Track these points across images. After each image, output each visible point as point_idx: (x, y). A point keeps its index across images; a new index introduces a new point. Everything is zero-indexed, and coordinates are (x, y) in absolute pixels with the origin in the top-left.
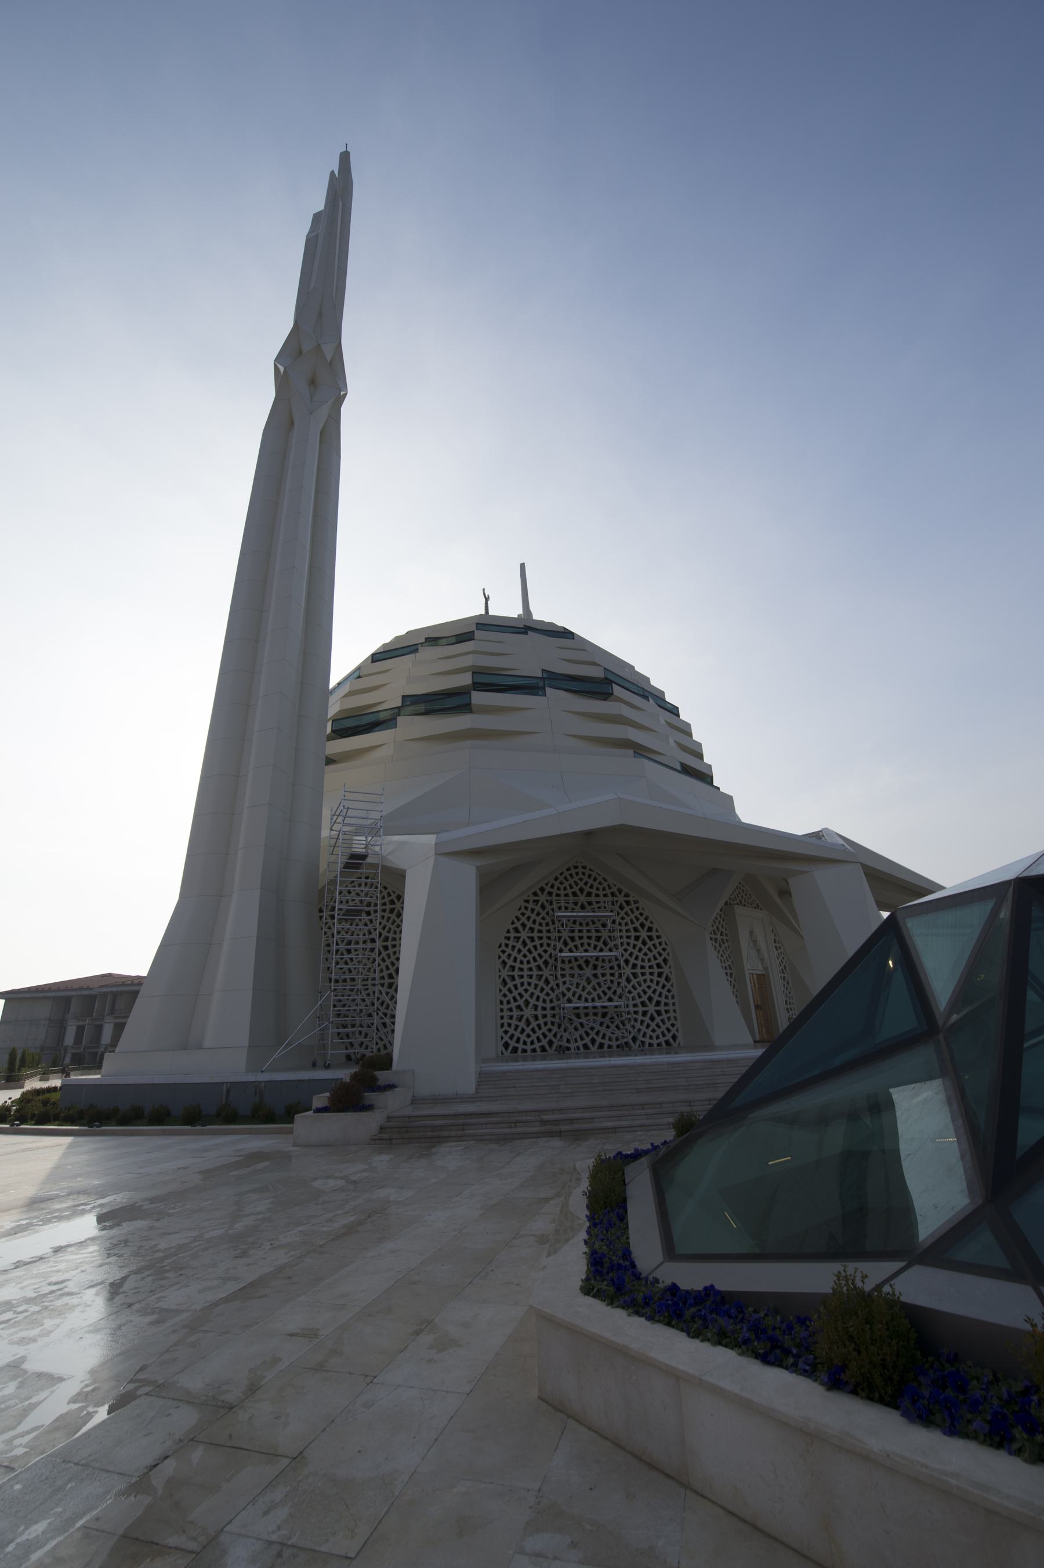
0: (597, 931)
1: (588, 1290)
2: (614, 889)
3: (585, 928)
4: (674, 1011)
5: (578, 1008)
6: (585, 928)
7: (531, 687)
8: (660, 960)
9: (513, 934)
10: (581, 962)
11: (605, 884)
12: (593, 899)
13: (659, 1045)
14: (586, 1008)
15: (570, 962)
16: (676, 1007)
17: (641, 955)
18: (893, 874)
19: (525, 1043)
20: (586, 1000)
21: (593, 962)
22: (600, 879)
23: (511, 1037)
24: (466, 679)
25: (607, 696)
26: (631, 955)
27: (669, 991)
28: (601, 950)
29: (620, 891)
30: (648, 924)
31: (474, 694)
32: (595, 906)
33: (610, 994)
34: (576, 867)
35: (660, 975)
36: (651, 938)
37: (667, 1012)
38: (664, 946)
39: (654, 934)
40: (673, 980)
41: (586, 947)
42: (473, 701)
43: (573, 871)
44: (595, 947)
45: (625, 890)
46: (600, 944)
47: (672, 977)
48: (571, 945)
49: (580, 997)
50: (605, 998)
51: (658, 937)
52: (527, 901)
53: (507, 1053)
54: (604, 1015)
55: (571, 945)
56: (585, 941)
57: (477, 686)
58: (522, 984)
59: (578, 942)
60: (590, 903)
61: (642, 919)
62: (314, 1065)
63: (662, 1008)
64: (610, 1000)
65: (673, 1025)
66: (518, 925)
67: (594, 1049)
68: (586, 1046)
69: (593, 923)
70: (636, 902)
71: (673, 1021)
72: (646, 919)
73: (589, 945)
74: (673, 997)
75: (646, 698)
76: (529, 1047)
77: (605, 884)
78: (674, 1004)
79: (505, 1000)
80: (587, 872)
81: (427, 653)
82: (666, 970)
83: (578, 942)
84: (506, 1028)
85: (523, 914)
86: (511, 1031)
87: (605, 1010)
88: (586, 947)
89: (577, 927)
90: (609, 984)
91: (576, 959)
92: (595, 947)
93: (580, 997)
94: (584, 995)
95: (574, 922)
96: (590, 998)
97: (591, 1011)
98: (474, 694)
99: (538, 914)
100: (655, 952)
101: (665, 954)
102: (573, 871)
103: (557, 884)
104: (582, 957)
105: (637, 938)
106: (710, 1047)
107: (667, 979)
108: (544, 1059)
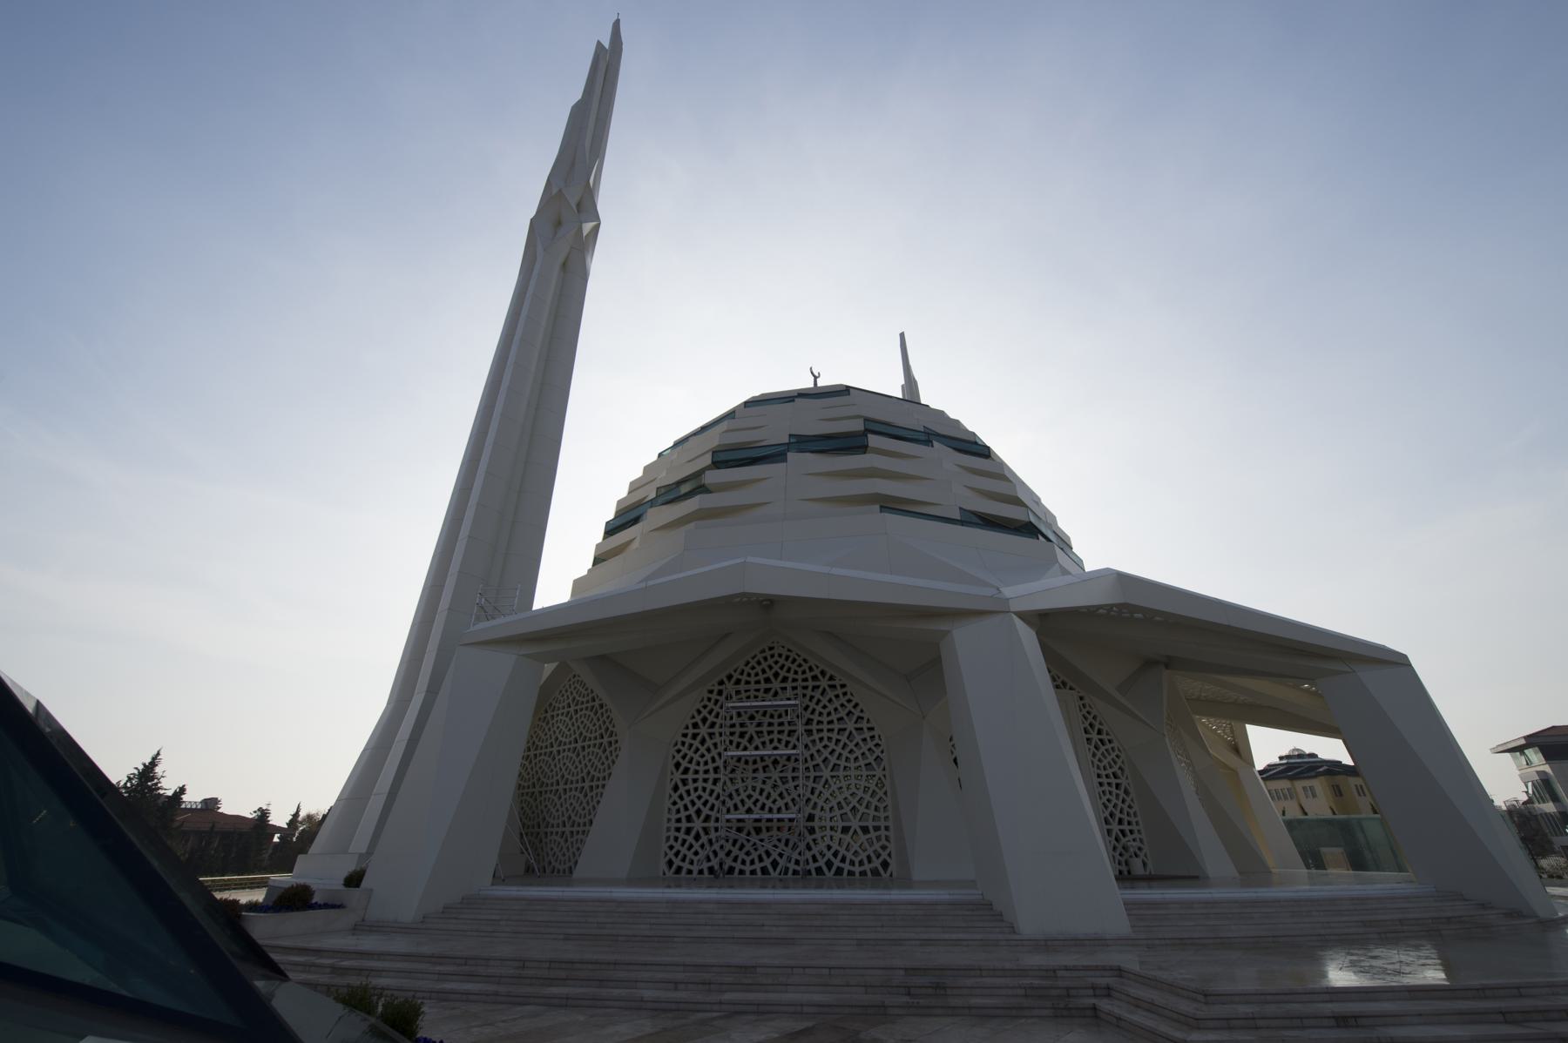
2: (817, 672)
3: (776, 721)
4: (887, 828)
6: (776, 721)
7: (775, 455)
8: (682, 790)
10: (769, 762)
11: (806, 667)
12: (742, 687)
13: (753, 872)
14: (769, 820)
15: (755, 762)
16: (1141, 827)
17: (845, 753)
18: (1233, 624)
19: (743, 862)
20: (771, 810)
22: (799, 660)
23: (677, 854)
24: (858, 426)
25: (864, 449)
27: (671, 847)
28: (745, 749)
29: (823, 673)
30: (691, 731)
32: (744, 695)
33: (749, 803)
35: (686, 771)
36: (704, 720)
37: (679, 820)
38: (877, 740)
39: (698, 719)
40: (1133, 794)
41: (776, 743)
45: (830, 672)
46: (744, 742)
47: (1131, 790)
48: (757, 741)
49: (763, 808)
50: (742, 809)
51: (699, 712)
52: (711, 692)
53: (670, 873)
56: (775, 736)
57: (717, 464)
58: (696, 789)
59: (767, 738)
61: (688, 740)
63: (684, 825)
64: (749, 811)
65: (884, 848)
66: (864, 725)
67: (829, 874)
68: (764, 871)
70: (843, 686)
71: (884, 842)
72: (685, 735)
73: (779, 741)
74: (668, 838)
75: (928, 443)
76: (748, 868)
77: (806, 667)
78: (886, 818)
80: (753, 663)
84: (671, 842)
85: (779, 741)
86: (677, 846)
88: (776, 743)
89: (767, 720)
91: (762, 759)
92: (738, 745)
93: (763, 808)
94: (769, 803)
95: (764, 714)
96: (775, 808)
97: (775, 824)
99: (696, 772)
100: (690, 754)
101: (877, 752)
106: (907, 883)
107: (1126, 792)
108: (819, 887)
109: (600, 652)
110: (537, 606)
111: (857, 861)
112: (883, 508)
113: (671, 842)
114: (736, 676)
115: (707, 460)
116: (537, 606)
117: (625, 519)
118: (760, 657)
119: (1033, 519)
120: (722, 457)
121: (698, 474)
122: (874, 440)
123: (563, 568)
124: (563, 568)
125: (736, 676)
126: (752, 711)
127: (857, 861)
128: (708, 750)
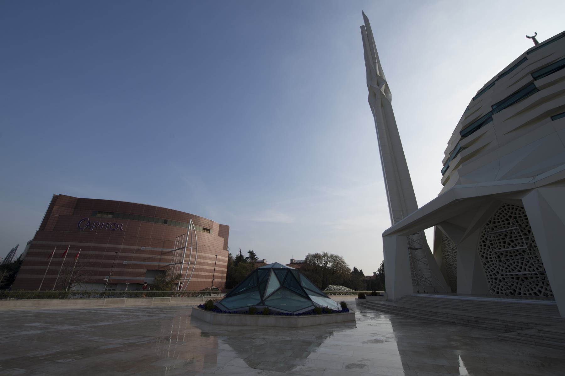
0: (503, 239)
1: (54, 195)
5: (525, 274)
9: (483, 244)
21: (504, 253)
24: (530, 78)
26: (484, 253)
28: (508, 248)
31: (535, 82)
32: (499, 227)
34: (504, 207)
39: (484, 239)
42: (537, 86)
43: (503, 209)
44: (504, 246)
46: (506, 245)
54: (518, 279)
55: (512, 244)
57: (535, 79)
60: (496, 227)
62: (418, 292)
69: (500, 235)
79: (487, 271)
80: (498, 214)
81: (491, 90)
82: (484, 260)
83: (516, 242)
84: (480, 250)
87: (517, 276)
90: (516, 264)
92: (504, 246)
98: (535, 82)
102: (503, 209)
103: (496, 217)
104: (520, 249)
105: (485, 245)
109: (442, 213)
110: (420, 206)
111: (521, 212)
112: (553, 118)
113: (480, 250)
114: (492, 221)
115: (530, 78)
116: (420, 206)
117: (472, 126)
118: (500, 211)
119: (6, 292)
120: (536, 75)
121: (531, 83)
122: (538, 83)
123: (428, 186)
124: (428, 186)
125: (492, 221)
126: (505, 233)
127: (521, 212)
128: (492, 261)
